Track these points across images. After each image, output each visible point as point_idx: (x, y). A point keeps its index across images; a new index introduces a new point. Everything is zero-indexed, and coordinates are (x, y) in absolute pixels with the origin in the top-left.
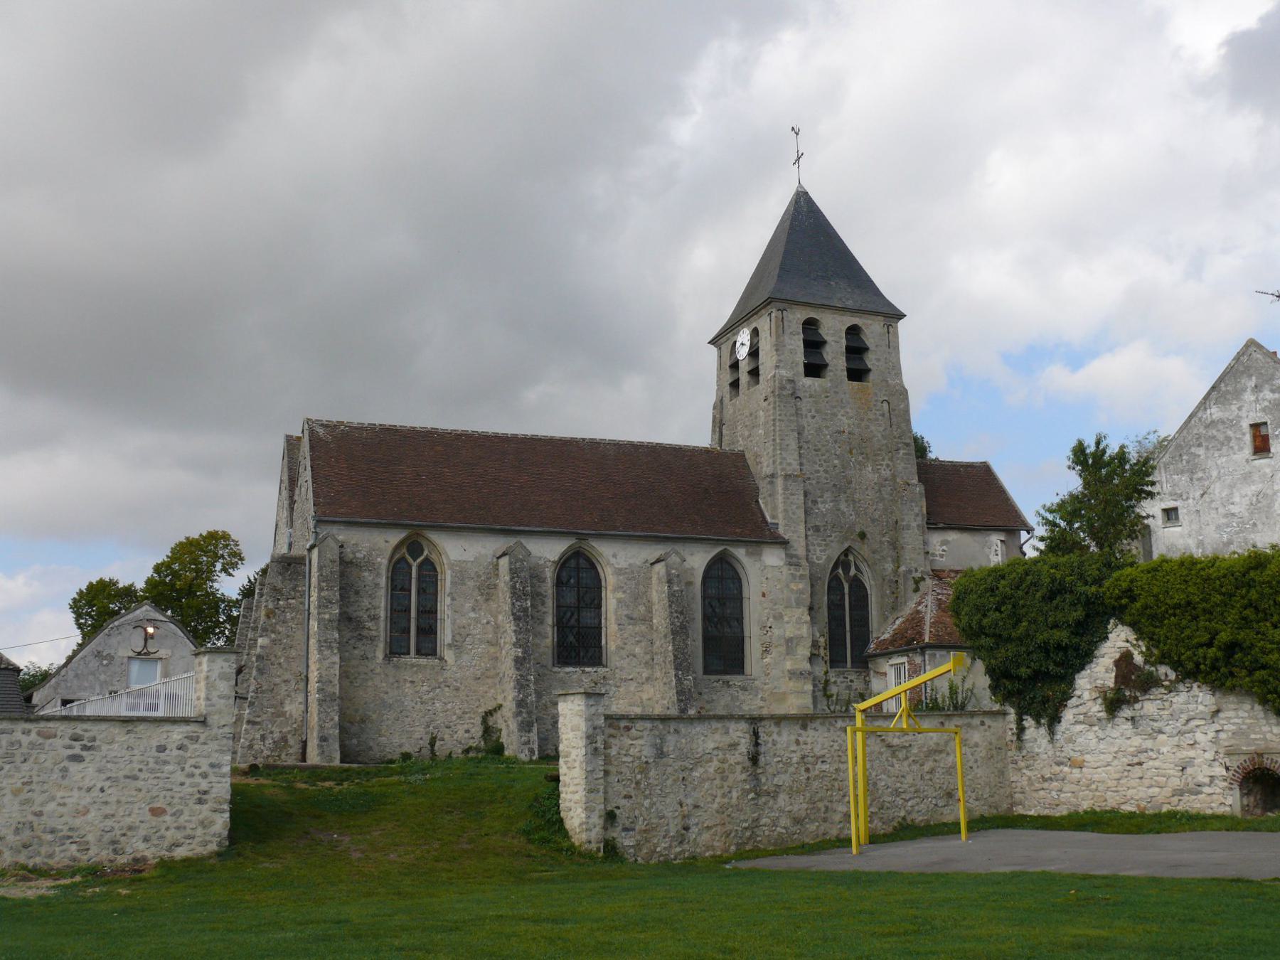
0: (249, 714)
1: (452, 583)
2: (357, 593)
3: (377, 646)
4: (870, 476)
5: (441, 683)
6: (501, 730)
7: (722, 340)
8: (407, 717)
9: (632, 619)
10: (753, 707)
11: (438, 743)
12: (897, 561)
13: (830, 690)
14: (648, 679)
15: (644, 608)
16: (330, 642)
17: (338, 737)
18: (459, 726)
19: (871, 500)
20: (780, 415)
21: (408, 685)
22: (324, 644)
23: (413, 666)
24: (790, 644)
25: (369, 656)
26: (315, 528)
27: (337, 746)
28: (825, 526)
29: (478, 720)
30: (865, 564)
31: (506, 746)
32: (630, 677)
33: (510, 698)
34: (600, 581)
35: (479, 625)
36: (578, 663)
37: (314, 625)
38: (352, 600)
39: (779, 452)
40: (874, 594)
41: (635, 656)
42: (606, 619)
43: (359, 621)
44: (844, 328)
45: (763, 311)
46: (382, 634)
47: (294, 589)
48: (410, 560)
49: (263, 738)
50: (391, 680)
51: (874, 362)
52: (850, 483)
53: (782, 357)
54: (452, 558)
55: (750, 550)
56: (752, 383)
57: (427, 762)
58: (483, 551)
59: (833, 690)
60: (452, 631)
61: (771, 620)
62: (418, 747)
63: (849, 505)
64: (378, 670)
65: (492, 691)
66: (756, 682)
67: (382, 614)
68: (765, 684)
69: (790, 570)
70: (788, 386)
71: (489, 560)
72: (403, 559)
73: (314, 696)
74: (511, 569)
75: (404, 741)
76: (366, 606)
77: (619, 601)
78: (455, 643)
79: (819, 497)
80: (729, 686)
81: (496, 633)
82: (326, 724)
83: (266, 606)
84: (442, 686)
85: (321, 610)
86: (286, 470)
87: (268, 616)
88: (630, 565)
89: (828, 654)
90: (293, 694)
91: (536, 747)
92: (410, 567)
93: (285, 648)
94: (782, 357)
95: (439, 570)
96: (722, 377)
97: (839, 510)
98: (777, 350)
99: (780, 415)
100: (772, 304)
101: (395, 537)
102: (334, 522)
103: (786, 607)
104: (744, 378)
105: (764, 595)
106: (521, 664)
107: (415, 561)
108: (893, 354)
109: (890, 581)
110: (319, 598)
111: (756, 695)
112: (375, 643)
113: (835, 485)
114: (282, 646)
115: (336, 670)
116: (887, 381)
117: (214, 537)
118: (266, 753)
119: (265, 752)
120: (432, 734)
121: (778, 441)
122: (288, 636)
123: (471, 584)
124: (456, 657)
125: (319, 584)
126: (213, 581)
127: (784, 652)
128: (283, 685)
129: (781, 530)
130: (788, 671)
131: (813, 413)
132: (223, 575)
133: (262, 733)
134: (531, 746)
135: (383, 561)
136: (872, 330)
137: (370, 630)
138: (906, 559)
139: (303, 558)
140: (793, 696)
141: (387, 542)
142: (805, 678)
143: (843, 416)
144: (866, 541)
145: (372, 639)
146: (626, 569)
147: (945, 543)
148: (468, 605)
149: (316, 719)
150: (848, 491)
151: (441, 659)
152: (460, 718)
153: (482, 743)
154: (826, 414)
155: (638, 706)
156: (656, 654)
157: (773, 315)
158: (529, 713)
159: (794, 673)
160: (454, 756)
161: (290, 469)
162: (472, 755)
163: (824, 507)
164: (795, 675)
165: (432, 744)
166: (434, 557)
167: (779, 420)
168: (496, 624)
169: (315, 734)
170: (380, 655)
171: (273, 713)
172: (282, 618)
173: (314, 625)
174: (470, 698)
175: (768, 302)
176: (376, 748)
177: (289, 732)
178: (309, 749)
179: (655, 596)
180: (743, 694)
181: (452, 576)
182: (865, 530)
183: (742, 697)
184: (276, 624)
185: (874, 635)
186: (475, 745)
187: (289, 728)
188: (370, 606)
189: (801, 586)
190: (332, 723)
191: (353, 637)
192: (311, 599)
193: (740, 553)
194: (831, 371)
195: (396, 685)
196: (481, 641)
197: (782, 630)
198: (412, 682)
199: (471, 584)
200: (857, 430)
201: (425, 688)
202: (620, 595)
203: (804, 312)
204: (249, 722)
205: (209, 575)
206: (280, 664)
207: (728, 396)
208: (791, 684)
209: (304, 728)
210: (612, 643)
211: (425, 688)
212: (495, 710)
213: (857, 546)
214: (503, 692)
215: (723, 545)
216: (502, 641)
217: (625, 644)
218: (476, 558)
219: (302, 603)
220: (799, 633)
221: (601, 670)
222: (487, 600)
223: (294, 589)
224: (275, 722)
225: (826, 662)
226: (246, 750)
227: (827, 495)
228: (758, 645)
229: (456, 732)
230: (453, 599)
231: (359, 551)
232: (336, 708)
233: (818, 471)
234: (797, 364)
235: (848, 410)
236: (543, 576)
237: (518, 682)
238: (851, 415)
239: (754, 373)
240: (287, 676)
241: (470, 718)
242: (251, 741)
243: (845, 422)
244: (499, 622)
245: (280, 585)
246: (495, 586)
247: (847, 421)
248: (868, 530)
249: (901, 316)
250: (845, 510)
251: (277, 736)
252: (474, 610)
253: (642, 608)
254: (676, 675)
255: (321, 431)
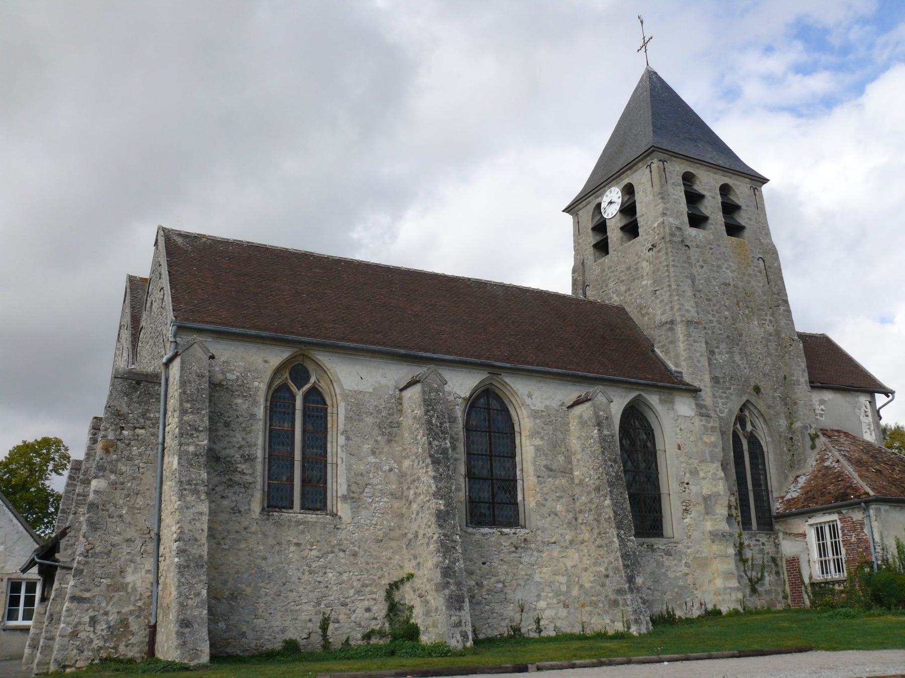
0: (75, 586)
1: (346, 418)
2: (227, 425)
3: (252, 496)
4: (757, 329)
5: (334, 546)
6: (411, 608)
7: (581, 206)
8: (291, 591)
9: (551, 470)
10: (678, 574)
11: (331, 627)
12: (791, 417)
13: (745, 555)
14: (571, 542)
15: (563, 458)
16: (196, 484)
17: (206, 620)
18: (357, 603)
19: (761, 354)
20: (674, 261)
21: (292, 548)
22: (186, 486)
23: (298, 523)
24: (708, 501)
25: (242, 509)
26: (175, 336)
27: (204, 634)
28: (724, 377)
29: (381, 595)
30: (761, 420)
31: (422, 628)
32: (553, 540)
33: (430, 564)
34: (512, 426)
35: (380, 473)
36: (493, 523)
37: (172, 462)
38: (220, 433)
39: (677, 298)
40: (771, 452)
41: (556, 515)
42: (522, 470)
43: (229, 462)
44: (718, 186)
45: (640, 165)
46: (259, 480)
47: (143, 415)
48: (294, 388)
49: (93, 621)
50: (271, 541)
51: (747, 220)
52: (741, 335)
53: (668, 205)
54: (345, 387)
55: (663, 397)
56: (624, 239)
57: (319, 649)
58: (384, 382)
59: (748, 554)
60: (348, 480)
61: (688, 475)
62: (307, 631)
63: (742, 358)
64: (253, 528)
65: (397, 557)
66: (680, 546)
67: (259, 454)
68: (688, 548)
69: (701, 421)
70: (677, 233)
71: (391, 393)
72: (284, 387)
73: (170, 560)
74: (425, 400)
75: (287, 623)
76: (238, 442)
77: (538, 449)
78: (352, 495)
79: (716, 347)
80: (653, 550)
81: (400, 483)
82: (190, 602)
83: (104, 437)
84: (336, 550)
85: (183, 441)
86: (128, 310)
87: (106, 450)
88: (546, 407)
89: (740, 514)
90: (138, 559)
91: (469, 629)
92: (293, 397)
93: (128, 495)
94: (668, 205)
95: (329, 402)
96: (581, 241)
97: (734, 362)
98: (663, 198)
99: (674, 261)
100: (654, 155)
101: (276, 357)
102: (199, 331)
103: (702, 461)
104: (614, 234)
105: (679, 448)
106: (445, 521)
107: (299, 390)
108: (761, 216)
109: (786, 438)
110: (181, 422)
111: (680, 561)
112: (250, 491)
113: (728, 337)
114: (125, 492)
115: (204, 524)
116: (760, 240)
117: (46, 442)
118: (97, 643)
119: (96, 642)
120: (324, 613)
121: (674, 287)
122: (134, 478)
123: (369, 420)
124: (353, 512)
125: (181, 405)
126: (47, 479)
127: (703, 511)
128: (124, 546)
129: (687, 379)
130: (710, 532)
131: (701, 263)
132: (54, 474)
133: (92, 614)
134: (464, 629)
135: (261, 386)
136: (741, 191)
137: (244, 474)
138: (800, 415)
139: (157, 376)
140: (718, 560)
141: (266, 361)
142: (727, 540)
143: (727, 268)
144: (761, 395)
145: (246, 486)
146: (542, 411)
147: (822, 402)
148: (366, 447)
149: (174, 593)
150: (740, 343)
151: (334, 515)
152: (358, 592)
153: (387, 625)
154: (713, 265)
155: (563, 575)
156: (581, 512)
157: (653, 166)
158: (459, 584)
159: (716, 535)
160: (352, 643)
161: (133, 307)
162: (374, 641)
163: (721, 358)
164: (716, 536)
165: (324, 627)
166: (323, 386)
167: (673, 266)
168: (400, 472)
169: (172, 616)
170: (256, 507)
171: (109, 586)
172: (126, 453)
173: (172, 462)
174: (371, 565)
175: (650, 152)
176: (250, 635)
177: (131, 613)
178: (160, 638)
179: (575, 443)
180: (667, 559)
181: (346, 410)
182: (759, 384)
183: (667, 563)
184: (117, 461)
185: (775, 495)
186: (377, 628)
187: (131, 608)
188: (243, 443)
189: (713, 439)
190: (198, 599)
191: (221, 483)
192: (167, 429)
193: (654, 399)
194: (712, 224)
195: (277, 548)
196: (383, 493)
197: (699, 487)
198: (298, 545)
199: (369, 420)
200: (740, 284)
201: (314, 553)
202: (538, 442)
203: (681, 166)
204: (73, 598)
205: (43, 473)
206: (121, 516)
207: (591, 258)
208: (715, 547)
209: (153, 607)
210: (531, 499)
211: (314, 553)
212: (402, 581)
213: (753, 399)
214: (415, 557)
215: (637, 390)
216: (412, 492)
217: (546, 500)
218: (374, 389)
219: (154, 435)
220: (716, 490)
221: (521, 532)
222: (389, 441)
223: (143, 415)
224: (111, 598)
225: (738, 523)
226: (66, 639)
227: (723, 346)
228: (679, 503)
229: (354, 611)
230: (348, 439)
231: (231, 371)
232: (204, 578)
233: (711, 322)
234: (682, 214)
235: (731, 264)
236: (454, 416)
237: (443, 544)
238: (734, 268)
239: (631, 230)
240: (131, 533)
241: (372, 593)
242: (76, 626)
243: (729, 275)
244: (404, 469)
245: (124, 409)
246: (399, 425)
247: (730, 274)
248: (762, 385)
249: (764, 181)
250: (740, 362)
251: (113, 618)
252: (374, 453)
253: (561, 458)
254: (618, 535)
255: (180, 241)
